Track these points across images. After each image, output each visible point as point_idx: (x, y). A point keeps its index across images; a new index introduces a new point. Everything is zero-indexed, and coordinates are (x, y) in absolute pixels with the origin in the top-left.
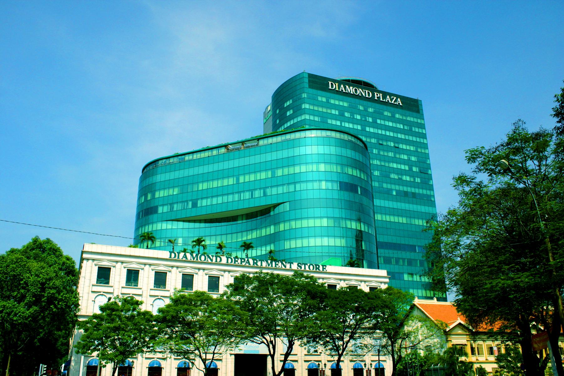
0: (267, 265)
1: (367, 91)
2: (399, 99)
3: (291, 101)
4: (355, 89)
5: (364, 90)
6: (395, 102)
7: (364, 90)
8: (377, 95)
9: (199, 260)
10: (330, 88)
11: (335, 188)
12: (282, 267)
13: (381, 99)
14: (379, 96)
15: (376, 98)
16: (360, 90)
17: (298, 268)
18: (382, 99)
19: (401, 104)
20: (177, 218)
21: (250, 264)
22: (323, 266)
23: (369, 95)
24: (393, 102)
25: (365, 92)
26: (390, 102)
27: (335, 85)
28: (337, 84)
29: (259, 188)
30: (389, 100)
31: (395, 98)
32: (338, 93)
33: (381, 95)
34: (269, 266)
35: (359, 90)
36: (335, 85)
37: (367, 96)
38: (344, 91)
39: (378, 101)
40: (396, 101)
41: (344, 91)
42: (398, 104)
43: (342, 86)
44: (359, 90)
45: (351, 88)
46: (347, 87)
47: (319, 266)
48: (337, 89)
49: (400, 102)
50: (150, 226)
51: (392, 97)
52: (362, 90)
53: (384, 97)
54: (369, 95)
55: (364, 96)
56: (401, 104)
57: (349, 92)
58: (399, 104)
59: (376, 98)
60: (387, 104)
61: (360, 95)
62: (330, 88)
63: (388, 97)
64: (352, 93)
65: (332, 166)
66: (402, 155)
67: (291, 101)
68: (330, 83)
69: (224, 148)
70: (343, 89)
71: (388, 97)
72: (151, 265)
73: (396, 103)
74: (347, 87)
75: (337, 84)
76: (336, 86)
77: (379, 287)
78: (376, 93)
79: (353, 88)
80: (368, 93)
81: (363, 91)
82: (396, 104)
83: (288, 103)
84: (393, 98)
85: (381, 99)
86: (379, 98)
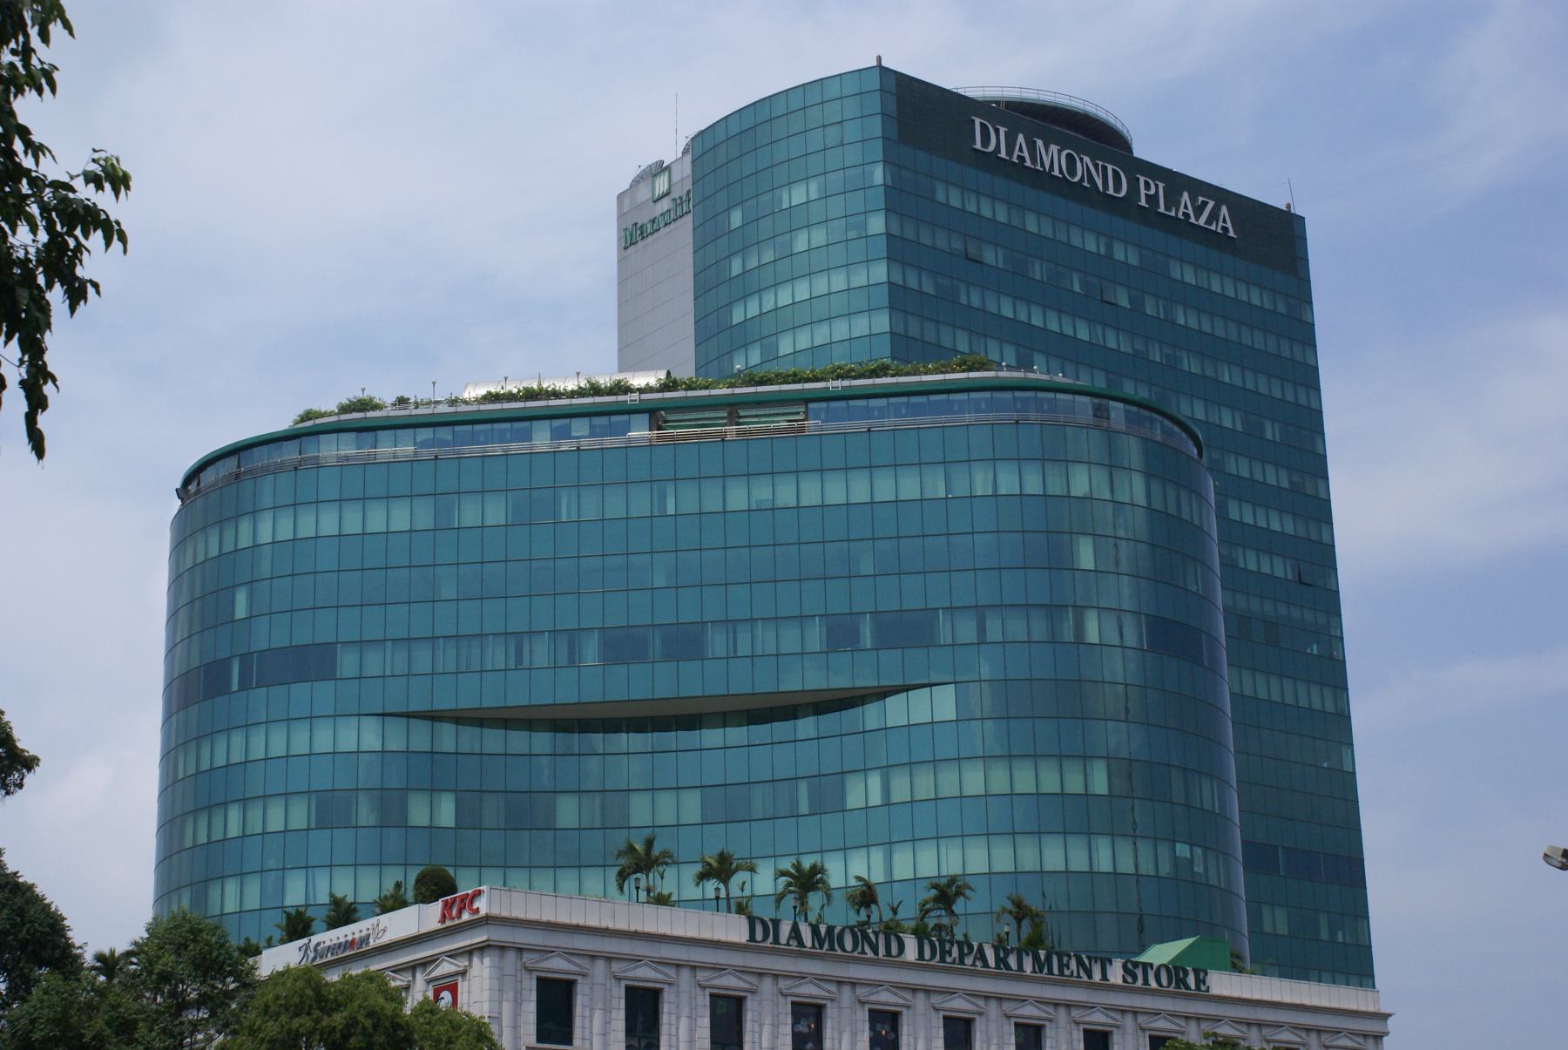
0: (817, 945)
1: (1110, 168)
2: (1224, 210)
3: (814, 189)
4: (1069, 157)
5: (1100, 163)
6: (1209, 222)
7: (1100, 163)
8: (1147, 186)
9: (1154, 984)
10: (978, 146)
11: (1131, 640)
12: (1079, 976)
13: (1162, 209)
14: (1152, 192)
15: (1143, 203)
16: (1086, 159)
17: (1125, 980)
18: (1166, 209)
19: (1231, 234)
20: (411, 710)
21: (986, 964)
22: (1196, 972)
23: (1118, 187)
24: (1202, 222)
25: (1105, 168)
26: (1193, 220)
27: (997, 132)
28: (1002, 130)
29: (822, 612)
30: (1190, 211)
31: (1211, 204)
32: (989, 162)
33: (1161, 185)
34: (821, 948)
35: (1081, 160)
36: (997, 132)
37: (1111, 191)
38: (1028, 163)
39: (1149, 216)
40: (1214, 217)
41: (1028, 163)
42: (1219, 231)
43: (1021, 138)
44: (1081, 160)
45: (1054, 148)
46: (1040, 143)
47: (1186, 973)
48: (1003, 154)
49: (1229, 225)
50: (237, 739)
51: (1201, 199)
52: (1092, 161)
53: (1172, 201)
54: (1118, 187)
55: (1101, 189)
56: (1231, 234)
57: (1047, 167)
58: (1225, 229)
59: (1143, 203)
60: (1181, 227)
61: (1086, 184)
62: (978, 146)
63: (1186, 196)
64: (1056, 173)
65: (1199, 568)
66: (1233, 458)
67: (814, 189)
68: (978, 121)
69: (646, 416)
70: (1026, 154)
71: (1186, 196)
72: (610, 958)
73: (1213, 227)
74: (1040, 143)
75: (1002, 130)
76: (998, 141)
77: (1242, 1042)
78: (1142, 179)
79: (1059, 152)
80: (1116, 175)
81: (1096, 166)
82: (1215, 232)
83: (798, 195)
84: (1205, 204)
85: (1162, 209)
86: (1152, 199)
